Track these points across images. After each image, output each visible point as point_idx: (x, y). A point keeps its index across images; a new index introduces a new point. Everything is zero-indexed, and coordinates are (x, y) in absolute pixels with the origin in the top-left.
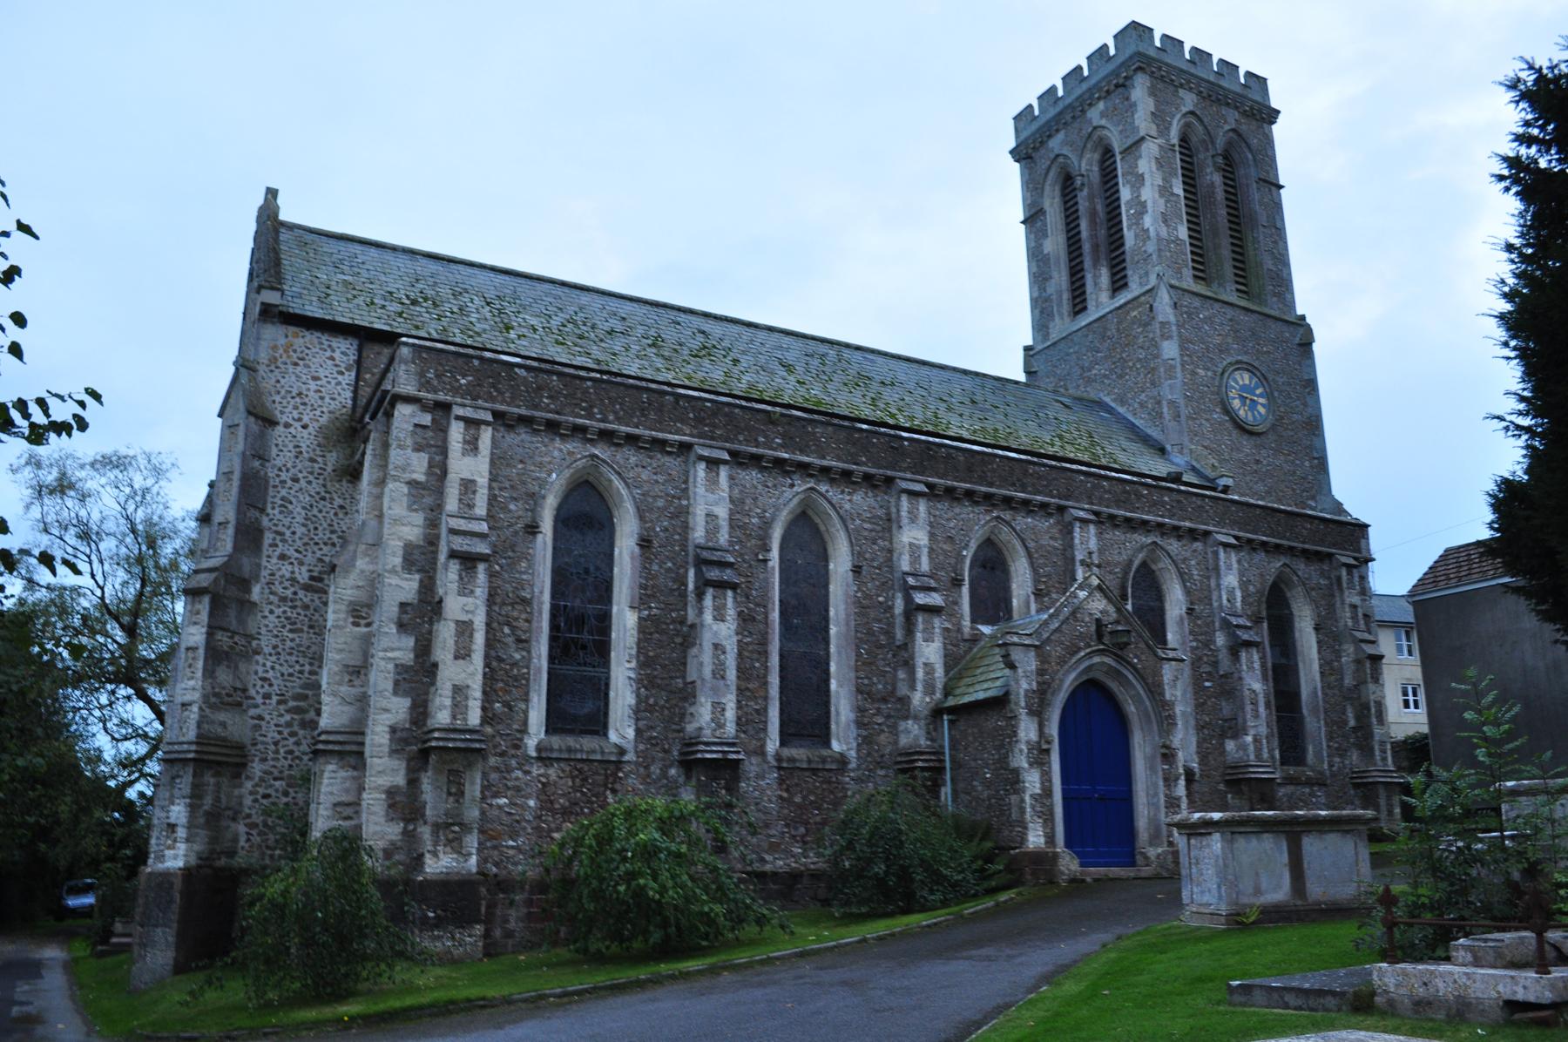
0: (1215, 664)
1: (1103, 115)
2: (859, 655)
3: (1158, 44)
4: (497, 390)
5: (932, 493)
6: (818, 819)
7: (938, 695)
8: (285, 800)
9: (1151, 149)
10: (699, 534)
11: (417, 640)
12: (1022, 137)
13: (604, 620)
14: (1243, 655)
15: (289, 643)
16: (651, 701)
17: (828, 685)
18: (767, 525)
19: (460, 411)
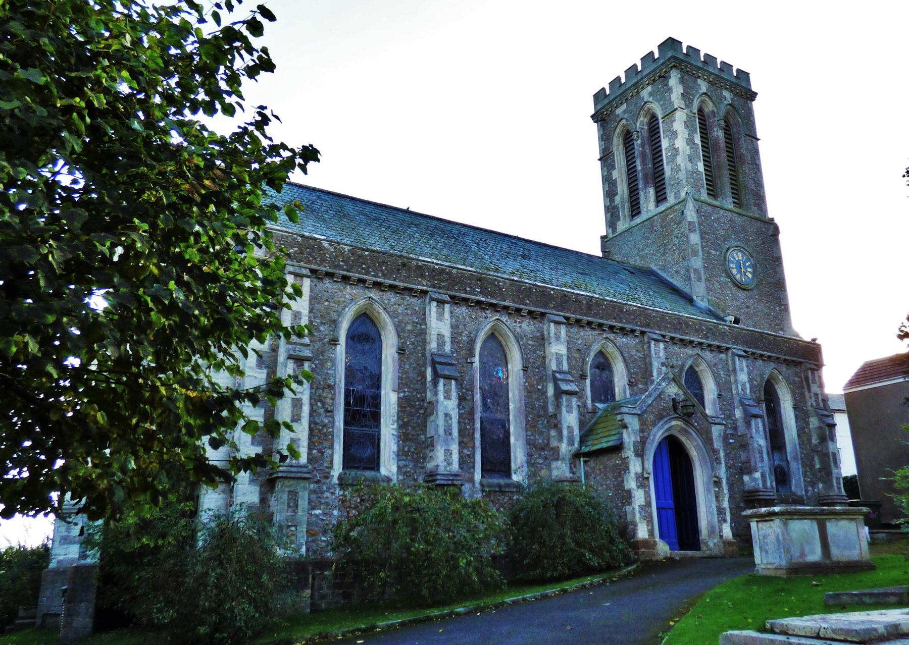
0: (735, 429)
1: (650, 94)
2: (527, 421)
4: (312, 256)
5: (568, 322)
7: (576, 445)
9: (680, 116)
10: (433, 346)
11: (265, 411)
12: (599, 107)
13: (377, 399)
14: (753, 423)
16: (406, 449)
18: (472, 342)
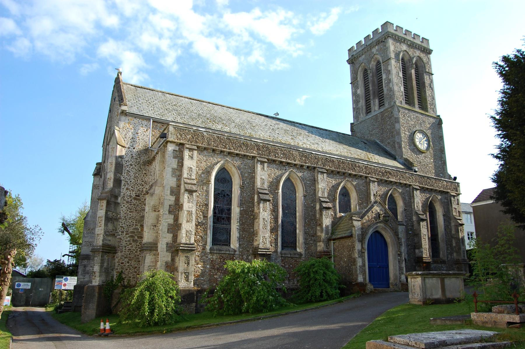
0: (413, 226)
2: (305, 222)
3: (395, 29)
6: (293, 272)
8: (128, 264)
13: (230, 210)
15: (129, 216)
17: (296, 231)
19: (188, 146)
